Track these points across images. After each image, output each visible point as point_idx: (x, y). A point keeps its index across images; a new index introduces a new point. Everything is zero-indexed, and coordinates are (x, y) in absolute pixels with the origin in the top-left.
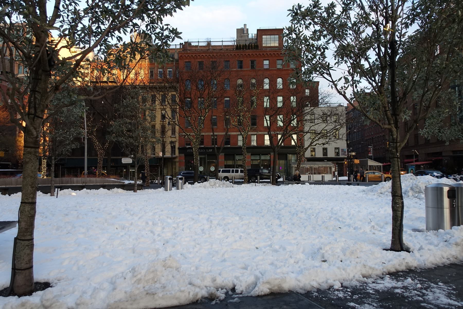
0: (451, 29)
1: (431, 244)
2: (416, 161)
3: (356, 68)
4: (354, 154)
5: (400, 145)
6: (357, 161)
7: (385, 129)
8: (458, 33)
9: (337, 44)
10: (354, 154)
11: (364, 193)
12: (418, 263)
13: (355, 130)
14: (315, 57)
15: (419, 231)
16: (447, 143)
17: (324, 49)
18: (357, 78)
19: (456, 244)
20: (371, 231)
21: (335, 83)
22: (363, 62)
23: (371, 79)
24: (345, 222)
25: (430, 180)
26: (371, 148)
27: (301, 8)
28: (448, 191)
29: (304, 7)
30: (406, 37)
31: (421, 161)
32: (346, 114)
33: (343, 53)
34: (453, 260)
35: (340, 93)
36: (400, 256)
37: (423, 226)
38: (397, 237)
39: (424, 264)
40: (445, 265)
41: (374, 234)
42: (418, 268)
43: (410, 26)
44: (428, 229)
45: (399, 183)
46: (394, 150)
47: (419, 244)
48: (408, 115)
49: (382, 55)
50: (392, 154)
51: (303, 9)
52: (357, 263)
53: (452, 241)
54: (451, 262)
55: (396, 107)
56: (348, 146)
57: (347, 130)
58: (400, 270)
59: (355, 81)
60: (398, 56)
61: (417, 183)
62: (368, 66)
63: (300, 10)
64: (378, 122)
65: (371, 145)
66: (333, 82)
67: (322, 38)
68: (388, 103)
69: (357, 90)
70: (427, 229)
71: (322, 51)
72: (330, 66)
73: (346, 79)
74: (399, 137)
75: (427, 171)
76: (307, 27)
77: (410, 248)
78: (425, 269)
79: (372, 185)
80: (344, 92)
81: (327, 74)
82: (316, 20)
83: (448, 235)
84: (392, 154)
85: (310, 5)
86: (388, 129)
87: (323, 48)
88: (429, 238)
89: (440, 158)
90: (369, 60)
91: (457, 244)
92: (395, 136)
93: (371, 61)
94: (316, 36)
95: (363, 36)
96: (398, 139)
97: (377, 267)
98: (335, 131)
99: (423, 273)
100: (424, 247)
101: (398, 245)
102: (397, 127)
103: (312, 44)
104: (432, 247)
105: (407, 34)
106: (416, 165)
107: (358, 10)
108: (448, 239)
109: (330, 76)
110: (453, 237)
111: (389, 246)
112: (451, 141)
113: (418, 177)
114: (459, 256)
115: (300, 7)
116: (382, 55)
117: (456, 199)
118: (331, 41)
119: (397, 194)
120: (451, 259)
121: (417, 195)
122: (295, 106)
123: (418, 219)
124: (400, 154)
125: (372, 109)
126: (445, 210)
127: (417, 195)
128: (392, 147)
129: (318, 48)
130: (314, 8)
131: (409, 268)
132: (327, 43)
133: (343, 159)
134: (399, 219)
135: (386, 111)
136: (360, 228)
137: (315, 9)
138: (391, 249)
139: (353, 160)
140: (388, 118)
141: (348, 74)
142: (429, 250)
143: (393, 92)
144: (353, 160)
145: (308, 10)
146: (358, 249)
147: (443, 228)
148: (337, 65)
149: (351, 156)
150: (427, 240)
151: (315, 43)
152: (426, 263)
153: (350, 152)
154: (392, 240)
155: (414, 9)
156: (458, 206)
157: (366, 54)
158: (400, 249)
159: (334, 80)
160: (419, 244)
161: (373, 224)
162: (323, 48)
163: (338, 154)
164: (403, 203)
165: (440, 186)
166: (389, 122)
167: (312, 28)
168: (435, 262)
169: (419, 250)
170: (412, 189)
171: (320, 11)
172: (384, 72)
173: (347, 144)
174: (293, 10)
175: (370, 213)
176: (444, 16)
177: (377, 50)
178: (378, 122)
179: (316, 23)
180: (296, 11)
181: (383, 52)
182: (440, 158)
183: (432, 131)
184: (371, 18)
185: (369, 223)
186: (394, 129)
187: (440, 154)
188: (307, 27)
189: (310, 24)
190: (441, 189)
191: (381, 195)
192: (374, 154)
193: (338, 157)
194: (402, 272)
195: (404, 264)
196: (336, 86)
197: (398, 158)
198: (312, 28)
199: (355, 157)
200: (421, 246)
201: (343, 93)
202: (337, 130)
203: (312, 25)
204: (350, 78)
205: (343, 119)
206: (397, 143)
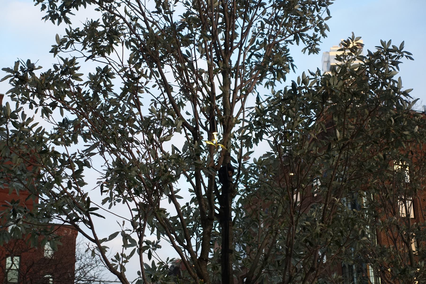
0: (329, 158)
3: (149, 213)
8: (340, 167)
9: (111, 158)
14: (58, 181)
17: (81, 165)
18: (150, 236)
21: (102, 244)
22: (164, 203)
23: (181, 243)
27: (33, 69)
29: (40, 67)
30: (251, 161)
33: (121, 179)
35: (113, 270)
43: (254, 145)
49: (203, 193)
51: (38, 74)
59: (148, 242)
60: (237, 198)
62: (175, 214)
63: (32, 74)
66: (96, 241)
67: (80, 138)
69: (153, 263)
71: (77, 168)
72: (92, 206)
73: (126, 237)
76: (46, 112)
81: (84, 221)
82: (67, 99)
85: (55, 66)
87: (78, 162)
90: (178, 200)
93: (182, 203)
94: (65, 133)
95: (167, 147)
103: (53, 151)
105: (252, 156)
107: (157, 92)
109: (92, 228)
115: (31, 67)
116: (203, 193)
118: (96, 150)
122: (16, 281)
129: (68, 163)
130: (63, 73)
132: (89, 152)
137: (64, 77)
141: (131, 228)
145: (48, 75)
148: (108, 204)
151: (60, 149)
155: (260, 112)
157: (171, 188)
159: (100, 238)
162: (78, 162)
167: (57, 116)
171: (76, 83)
172: (208, 229)
174: (15, 71)
176: (313, 135)
177: (194, 180)
179: (66, 106)
180: (21, 73)
181: (207, 185)
184: (183, 112)
188: (46, 112)
189: (53, 105)
196: (103, 250)
198: (57, 116)
201: (119, 270)
203: (57, 109)
204: (135, 236)
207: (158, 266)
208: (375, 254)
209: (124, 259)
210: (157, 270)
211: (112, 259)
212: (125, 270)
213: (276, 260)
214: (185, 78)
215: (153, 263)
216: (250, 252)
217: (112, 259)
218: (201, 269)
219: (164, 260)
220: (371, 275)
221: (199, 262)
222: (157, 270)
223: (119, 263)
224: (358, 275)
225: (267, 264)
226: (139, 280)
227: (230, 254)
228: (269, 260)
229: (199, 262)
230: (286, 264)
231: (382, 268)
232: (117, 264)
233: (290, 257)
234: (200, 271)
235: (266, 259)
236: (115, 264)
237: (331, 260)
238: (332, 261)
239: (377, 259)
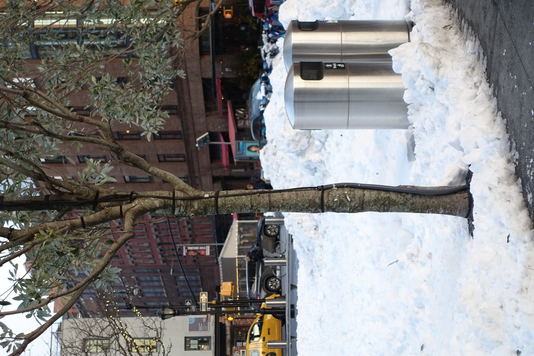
1: (443, 122)
2: (227, 139)
4: (204, 297)
5: (182, 191)
6: (226, 289)
7: (134, 225)
10: (204, 297)
11: (316, 274)
12: (497, 155)
13: (135, 292)
15: (412, 145)
16: (181, 73)
19: (438, 68)
20: (423, 264)
24: (405, 332)
25: (277, 114)
26: (188, 249)
28: (304, 78)
31: (227, 128)
32: (85, 316)
34: (479, 76)
36: (483, 198)
37: (399, 136)
38: (435, 201)
39: (498, 142)
40: (494, 94)
41: (430, 256)
42: (509, 155)
44: (406, 125)
45: (286, 194)
46: (196, 204)
47: (445, 147)
48: (99, 168)
50: (205, 209)
52: (517, 310)
53: (431, 75)
54: (484, 80)
55: (73, 198)
56: (180, 311)
57: (134, 315)
58: (521, 198)
61: (286, 141)
64: (114, 245)
65: (181, 249)
68: (58, 219)
69: (16, 299)
70: (406, 127)
74: (158, 193)
75: (254, 112)
77: (461, 171)
78: (510, 139)
79: (294, 253)
80: (18, 338)
83: (417, 84)
84: (205, 209)
86: (134, 220)
88: (427, 125)
89: (218, 83)
91: (438, 66)
92: (157, 203)
96: (166, 194)
97: (521, 258)
98: (134, 350)
99: (521, 146)
100: (453, 140)
101: (455, 199)
102: (131, 198)
104: (451, 121)
106: (238, 137)
108: (427, 83)
110: (419, 72)
111: (460, 221)
112: (176, 66)
113: (269, 136)
114: (467, 63)
117: (324, 61)
119: (318, 200)
120: (476, 79)
121: (317, 143)
123: (379, 145)
124: (206, 190)
125: (75, 261)
126: (352, 86)
127: (317, 143)
128: (186, 209)
131: (513, 177)
133: (220, 328)
134: (383, 194)
135: (83, 224)
136: (419, 291)
138: (469, 216)
139: (222, 299)
140: (104, 220)
142: (459, 127)
143: (29, 205)
144: (222, 299)
146: (477, 306)
147: (401, 92)
149: (210, 305)
150: (434, 129)
152: (494, 136)
153: (198, 306)
154: (444, 213)
156: (342, 57)
158: (466, 195)
160: (445, 147)
161: (403, 257)
163: (203, 341)
164: (340, 186)
165: (292, 95)
166: (114, 217)
168: (488, 116)
169: (462, 149)
170: (301, 153)
173: (174, 315)
175: (374, 263)
178: (114, 245)
182: (218, 83)
183: (147, 107)
185: (402, 268)
186: (137, 204)
187: (207, 84)
190: (299, 93)
191: (320, 230)
192: (204, 242)
193: (213, 341)
194: (525, 194)
195: (503, 188)
197: (217, 197)
199: (214, 291)
200: (452, 144)
202: (131, 345)
205: (100, 325)
206: (174, 199)
207: (18, 293)
208: (15, 16)
209: (8, 335)
210: (25, 294)
211: (7, 352)
212: (22, 334)
213: (14, 142)
214: (151, 290)
215: (16, 299)
216: (5, 174)
217: (7, 352)
218: (22, 237)
219: (12, 283)
220: (41, 24)
221: (13, 239)
222: (25, 294)
223: (13, 341)
224: (43, 38)
225: (17, 153)
226: (38, 316)
227: (4, 200)
228: (13, 150)
229: (13, 239)
230: (18, 128)
231: (33, 8)
232: (13, 344)
233: (8, 123)
234: (24, 238)
235: (11, 154)
236: (14, 347)
237: (16, 72)
238: (17, 71)
239: (21, 14)
